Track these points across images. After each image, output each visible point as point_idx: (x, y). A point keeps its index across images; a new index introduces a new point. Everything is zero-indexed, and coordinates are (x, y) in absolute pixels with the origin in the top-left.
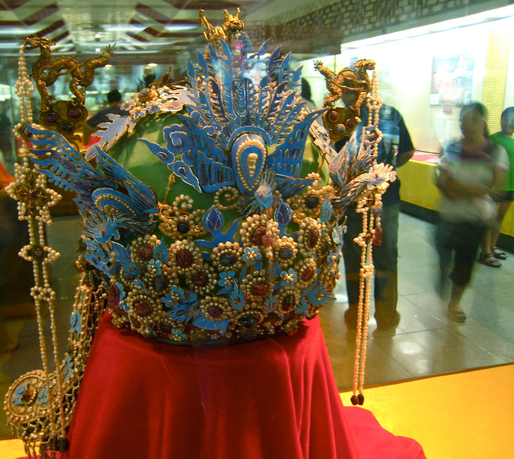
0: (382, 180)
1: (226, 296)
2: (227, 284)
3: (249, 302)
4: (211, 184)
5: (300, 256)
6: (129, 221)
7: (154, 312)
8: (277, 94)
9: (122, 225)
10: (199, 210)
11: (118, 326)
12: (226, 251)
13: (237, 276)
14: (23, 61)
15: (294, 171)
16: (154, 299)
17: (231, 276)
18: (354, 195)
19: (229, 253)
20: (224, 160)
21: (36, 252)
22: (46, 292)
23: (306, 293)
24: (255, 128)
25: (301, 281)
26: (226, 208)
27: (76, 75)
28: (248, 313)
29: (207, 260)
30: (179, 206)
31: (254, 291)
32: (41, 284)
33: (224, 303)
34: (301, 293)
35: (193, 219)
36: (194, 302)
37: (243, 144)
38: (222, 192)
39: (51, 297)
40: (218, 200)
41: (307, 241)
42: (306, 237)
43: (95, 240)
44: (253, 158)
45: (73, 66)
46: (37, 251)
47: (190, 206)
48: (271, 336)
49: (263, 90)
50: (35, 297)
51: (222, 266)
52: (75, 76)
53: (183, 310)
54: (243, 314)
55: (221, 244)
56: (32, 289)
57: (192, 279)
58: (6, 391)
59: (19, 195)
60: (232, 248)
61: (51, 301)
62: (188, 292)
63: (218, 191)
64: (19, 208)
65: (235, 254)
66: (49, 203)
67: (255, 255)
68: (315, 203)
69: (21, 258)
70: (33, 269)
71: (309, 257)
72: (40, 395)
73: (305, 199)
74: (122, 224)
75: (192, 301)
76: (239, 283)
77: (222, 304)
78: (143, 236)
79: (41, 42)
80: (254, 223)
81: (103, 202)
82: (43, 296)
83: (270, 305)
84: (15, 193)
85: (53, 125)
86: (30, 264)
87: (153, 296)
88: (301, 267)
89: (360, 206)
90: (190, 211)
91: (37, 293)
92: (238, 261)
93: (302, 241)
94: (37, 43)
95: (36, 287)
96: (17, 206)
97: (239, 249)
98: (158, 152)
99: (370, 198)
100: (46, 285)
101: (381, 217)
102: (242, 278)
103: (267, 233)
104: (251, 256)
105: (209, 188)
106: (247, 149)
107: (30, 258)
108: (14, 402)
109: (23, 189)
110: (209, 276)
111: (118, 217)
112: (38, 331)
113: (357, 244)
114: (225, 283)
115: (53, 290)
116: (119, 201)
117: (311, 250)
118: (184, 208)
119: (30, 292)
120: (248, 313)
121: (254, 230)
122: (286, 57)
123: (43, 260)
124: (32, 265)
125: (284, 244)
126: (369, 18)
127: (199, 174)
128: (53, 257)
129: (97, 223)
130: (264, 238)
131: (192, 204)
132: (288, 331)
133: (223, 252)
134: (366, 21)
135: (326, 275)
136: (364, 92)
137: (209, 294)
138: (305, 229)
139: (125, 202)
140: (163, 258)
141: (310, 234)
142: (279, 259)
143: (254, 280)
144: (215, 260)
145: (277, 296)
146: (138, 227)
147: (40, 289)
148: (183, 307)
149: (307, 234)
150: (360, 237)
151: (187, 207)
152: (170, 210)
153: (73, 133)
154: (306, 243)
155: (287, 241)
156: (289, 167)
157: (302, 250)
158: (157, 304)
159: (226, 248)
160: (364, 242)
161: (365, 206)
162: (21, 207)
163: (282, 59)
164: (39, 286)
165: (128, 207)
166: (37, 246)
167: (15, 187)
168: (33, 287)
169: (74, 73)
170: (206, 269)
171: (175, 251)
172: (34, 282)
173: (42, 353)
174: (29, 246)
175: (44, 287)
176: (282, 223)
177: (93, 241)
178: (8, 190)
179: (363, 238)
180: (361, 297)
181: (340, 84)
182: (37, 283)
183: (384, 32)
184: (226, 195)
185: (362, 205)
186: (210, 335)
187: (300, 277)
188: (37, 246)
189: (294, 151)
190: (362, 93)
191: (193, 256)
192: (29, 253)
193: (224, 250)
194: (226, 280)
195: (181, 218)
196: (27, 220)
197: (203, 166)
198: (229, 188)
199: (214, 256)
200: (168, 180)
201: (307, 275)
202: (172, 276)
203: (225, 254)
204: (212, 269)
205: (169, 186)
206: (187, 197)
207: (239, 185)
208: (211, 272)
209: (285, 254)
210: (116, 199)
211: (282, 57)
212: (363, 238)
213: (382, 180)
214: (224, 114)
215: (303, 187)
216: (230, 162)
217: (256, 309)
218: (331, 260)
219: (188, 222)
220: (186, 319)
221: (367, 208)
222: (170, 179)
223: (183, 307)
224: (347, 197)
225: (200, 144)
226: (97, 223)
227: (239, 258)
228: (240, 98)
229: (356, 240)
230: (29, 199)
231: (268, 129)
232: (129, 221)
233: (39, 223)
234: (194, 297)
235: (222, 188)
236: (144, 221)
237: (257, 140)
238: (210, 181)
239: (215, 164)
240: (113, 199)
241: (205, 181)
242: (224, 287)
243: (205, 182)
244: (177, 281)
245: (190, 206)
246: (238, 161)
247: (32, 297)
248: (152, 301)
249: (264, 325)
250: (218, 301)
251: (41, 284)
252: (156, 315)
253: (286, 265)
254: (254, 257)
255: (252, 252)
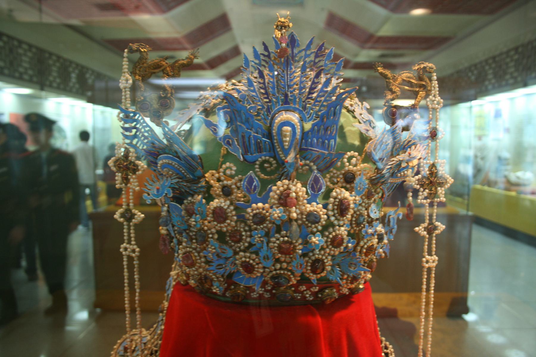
0: (414, 158)
1: (257, 253)
2: (257, 242)
3: (278, 261)
4: (251, 154)
5: (329, 225)
6: (181, 182)
7: (198, 264)
8: (315, 80)
9: (175, 185)
10: (240, 176)
11: (182, 283)
12: (258, 211)
13: (267, 235)
14: (127, 62)
15: (329, 146)
16: (199, 253)
17: (261, 235)
18: (389, 172)
19: (260, 213)
20: (264, 134)
21: (126, 215)
22: (132, 249)
23: (338, 260)
24: (292, 107)
25: (330, 247)
26: (268, 177)
27: (166, 72)
28: (278, 272)
29: (241, 219)
30: (224, 173)
31: (280, 249)
32: (129, 243)
33: (255, 259)
34: (332, 260)
35: (236, 184)
36: (231, 257)
37: (279, 119)
38: (261, 161)
39: (136, 253)
40: (259, 168)
41: (337, 209)
42: (336, 205)
43: (151, 195)
44: (287, 131)
45: (163, 65)
46: (127, 213)
47: (233, 172)
48: (310, 303)
49: (303, 76)
50: (124, 253)
51: (254, 225)
52: (165, 73)
53: (221, 265)
54: (274, 272)
55: (254, 205)
56: (122, 246)
57: (230, 236)
58: (115, 343)
59: (117, 167)
60: (263, 209)
61: (137, 256)
62: (225, 247)
63: (257, 160)
64: (116, 178)
65: (265, 214)
66: (137, 173)
67: (280, 215)
68: (351, 178)
69: (116, 220)
70: (123, 229)
71: (340, 226)
72: (137, 349)
73: (343, 174)
74: (175, 184)
75: (229, 256)
76: (268, 242)
77: (254, 260)
78: (192, 196)
79: (140, 47)
80: (283, 187)
81: (163, 166)
82: (130, 252)
83: (297, 267)
84: (115, 166)
85: (146, 111)
86: (122, 224)
87: (198, 249)
88: (330, 233)
89: (420, 197)
90: (232, 177)
91: (126, 249)
92: (267, 220)
93: (331, 209)
94: (136, 48)
95: (125, 244)
96: (115, 176)
97: (269, 210)
98: (211, 127)
99: (432, 191)
100: (133, 243)
101: (412, 192)
102: (271, 237)
103: (291, 195)
104: (276, 215)
105: (249, 157)
106: (282, 123)
107: (122, 220)
108: (118, 353)
109: (120, 162)
110: (244, 233)
111: (172, 178)
112: (124, 283)
113: (417, 233)
114: (256, 240)
115: (139, 247)
116: (176, 166)
117: (342, 218)
118: (228, 174)
119: (120, 248)
120: (278, 272)
121: (282, 193)
122: (329, 51)
123: (131, 222)
124: (123, 225)
125: (312, 209)
126: (511, 74)
127: (240, 144)
128: (139, 219)
129: (154, 182)
130: (289, 200)
131: (235, 171)
132: (325, 299)
133: (255, 212)
134: (508, 77)
135: (362, 247)
136: (422, 91)
137: (244, 251)
138: (335, 198)
139: (181, 167)
140: (202, 213)
141: (340, 203)
142: (307, 222)
143: (282, 239)
144: (249, 220)
145: (307, 259)
146: (188, 187)
147: (128, 246)
148: (221, 262)
149: (337, 203)
150: (421, 227)
151: (231, 173)
152: (217, 175)
153: (162, 118)
154: (336, 212)
155: (316, 207)
156: (323, 142)
157: (333, 219)
158: (201, 258)
159: (258, 208)
160: (425, 233)
161: (426, 198)
162: (119, 177)
163: (326, 53)
164: (128, 243)
165: (183, 171)
166: (128, 210)
167: (115, 160)
168: (122, 244)
169: (165, 71)
170: (241, 228)
171: (212, 208)
172: (124, 240)
173: (126, 302)
174: (122, 210)
175: (131, 244)
176: (315, 192)
177: (149, 196)
178: (110, 163)
179: (425, 228)
180: (424, 287)
181: (399, 84)
182: (126, 241)
183: (525, 85)
184: (266, 165)
185: (423, 196)
186: (250, 293)
187: (329, 243)
188: (128, 210)
189: (328, 127)
190: (421, 93)
191: (228, 213)
192: (122, 215)
193: (256, 210)
194: (257, 238)
195: (225, 182)
196: (122, 187)
197: (243, 137)
198: (267, 158)
199: (248, 216)
200: (220, 152)
201: (336, 242)
202: (211, 231)
203: (256, 214)
204: (247, 228)
205: (221, 157)
206: (232, 165)
207: (277, 156)
208: (246, 231)
209: (312, 218)
210: (173, 164)
211: (326, 51)
212: (425, 228)
213: (414, 158)
214: (268, 96)
215: (335, 161)
216: (269, 135)
217: (286, 269)
218: (366, 232)
219: (231, 186)
220: (225, 273)
221: (429, 201)
222: (222, 151)
223: (221, 262)
224: (382, 173)
225: (241, 118)
226: (154, 182)
227: (269, 218)
228: (282, 82)
229: (417, 229)
230: (123, 171)
231: (305, 108)
232: (181, 182)
233: (131, 190)
234: (230, 253)
235: (261, 158)
236: (194, 184)
237: (294, 117)
238: (250, 150)
239: (254, 135)
240: (171, 164)
241: (246, 150)
242: (255, 245)
243: (246, 152)
244: (216, 236)
245: (233, 172)
246: (275, 134)
247: (121, 253)
248: (196, 254)
249: (299, 289)
250: (249, 258)
251: (129, 243)
252: (200, 267)
253: (315, 230)
254: (279, 217)
255: (277, 213)
